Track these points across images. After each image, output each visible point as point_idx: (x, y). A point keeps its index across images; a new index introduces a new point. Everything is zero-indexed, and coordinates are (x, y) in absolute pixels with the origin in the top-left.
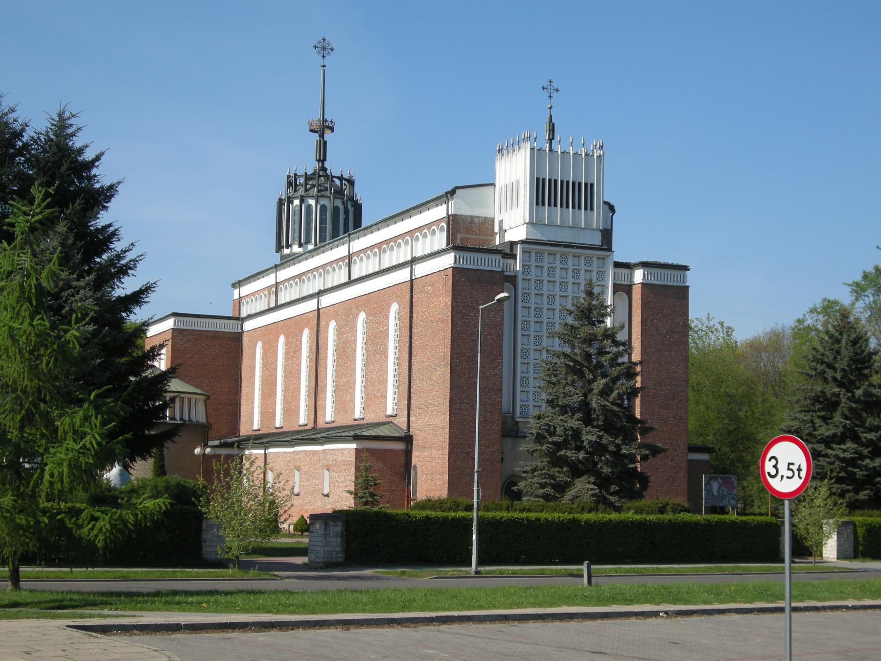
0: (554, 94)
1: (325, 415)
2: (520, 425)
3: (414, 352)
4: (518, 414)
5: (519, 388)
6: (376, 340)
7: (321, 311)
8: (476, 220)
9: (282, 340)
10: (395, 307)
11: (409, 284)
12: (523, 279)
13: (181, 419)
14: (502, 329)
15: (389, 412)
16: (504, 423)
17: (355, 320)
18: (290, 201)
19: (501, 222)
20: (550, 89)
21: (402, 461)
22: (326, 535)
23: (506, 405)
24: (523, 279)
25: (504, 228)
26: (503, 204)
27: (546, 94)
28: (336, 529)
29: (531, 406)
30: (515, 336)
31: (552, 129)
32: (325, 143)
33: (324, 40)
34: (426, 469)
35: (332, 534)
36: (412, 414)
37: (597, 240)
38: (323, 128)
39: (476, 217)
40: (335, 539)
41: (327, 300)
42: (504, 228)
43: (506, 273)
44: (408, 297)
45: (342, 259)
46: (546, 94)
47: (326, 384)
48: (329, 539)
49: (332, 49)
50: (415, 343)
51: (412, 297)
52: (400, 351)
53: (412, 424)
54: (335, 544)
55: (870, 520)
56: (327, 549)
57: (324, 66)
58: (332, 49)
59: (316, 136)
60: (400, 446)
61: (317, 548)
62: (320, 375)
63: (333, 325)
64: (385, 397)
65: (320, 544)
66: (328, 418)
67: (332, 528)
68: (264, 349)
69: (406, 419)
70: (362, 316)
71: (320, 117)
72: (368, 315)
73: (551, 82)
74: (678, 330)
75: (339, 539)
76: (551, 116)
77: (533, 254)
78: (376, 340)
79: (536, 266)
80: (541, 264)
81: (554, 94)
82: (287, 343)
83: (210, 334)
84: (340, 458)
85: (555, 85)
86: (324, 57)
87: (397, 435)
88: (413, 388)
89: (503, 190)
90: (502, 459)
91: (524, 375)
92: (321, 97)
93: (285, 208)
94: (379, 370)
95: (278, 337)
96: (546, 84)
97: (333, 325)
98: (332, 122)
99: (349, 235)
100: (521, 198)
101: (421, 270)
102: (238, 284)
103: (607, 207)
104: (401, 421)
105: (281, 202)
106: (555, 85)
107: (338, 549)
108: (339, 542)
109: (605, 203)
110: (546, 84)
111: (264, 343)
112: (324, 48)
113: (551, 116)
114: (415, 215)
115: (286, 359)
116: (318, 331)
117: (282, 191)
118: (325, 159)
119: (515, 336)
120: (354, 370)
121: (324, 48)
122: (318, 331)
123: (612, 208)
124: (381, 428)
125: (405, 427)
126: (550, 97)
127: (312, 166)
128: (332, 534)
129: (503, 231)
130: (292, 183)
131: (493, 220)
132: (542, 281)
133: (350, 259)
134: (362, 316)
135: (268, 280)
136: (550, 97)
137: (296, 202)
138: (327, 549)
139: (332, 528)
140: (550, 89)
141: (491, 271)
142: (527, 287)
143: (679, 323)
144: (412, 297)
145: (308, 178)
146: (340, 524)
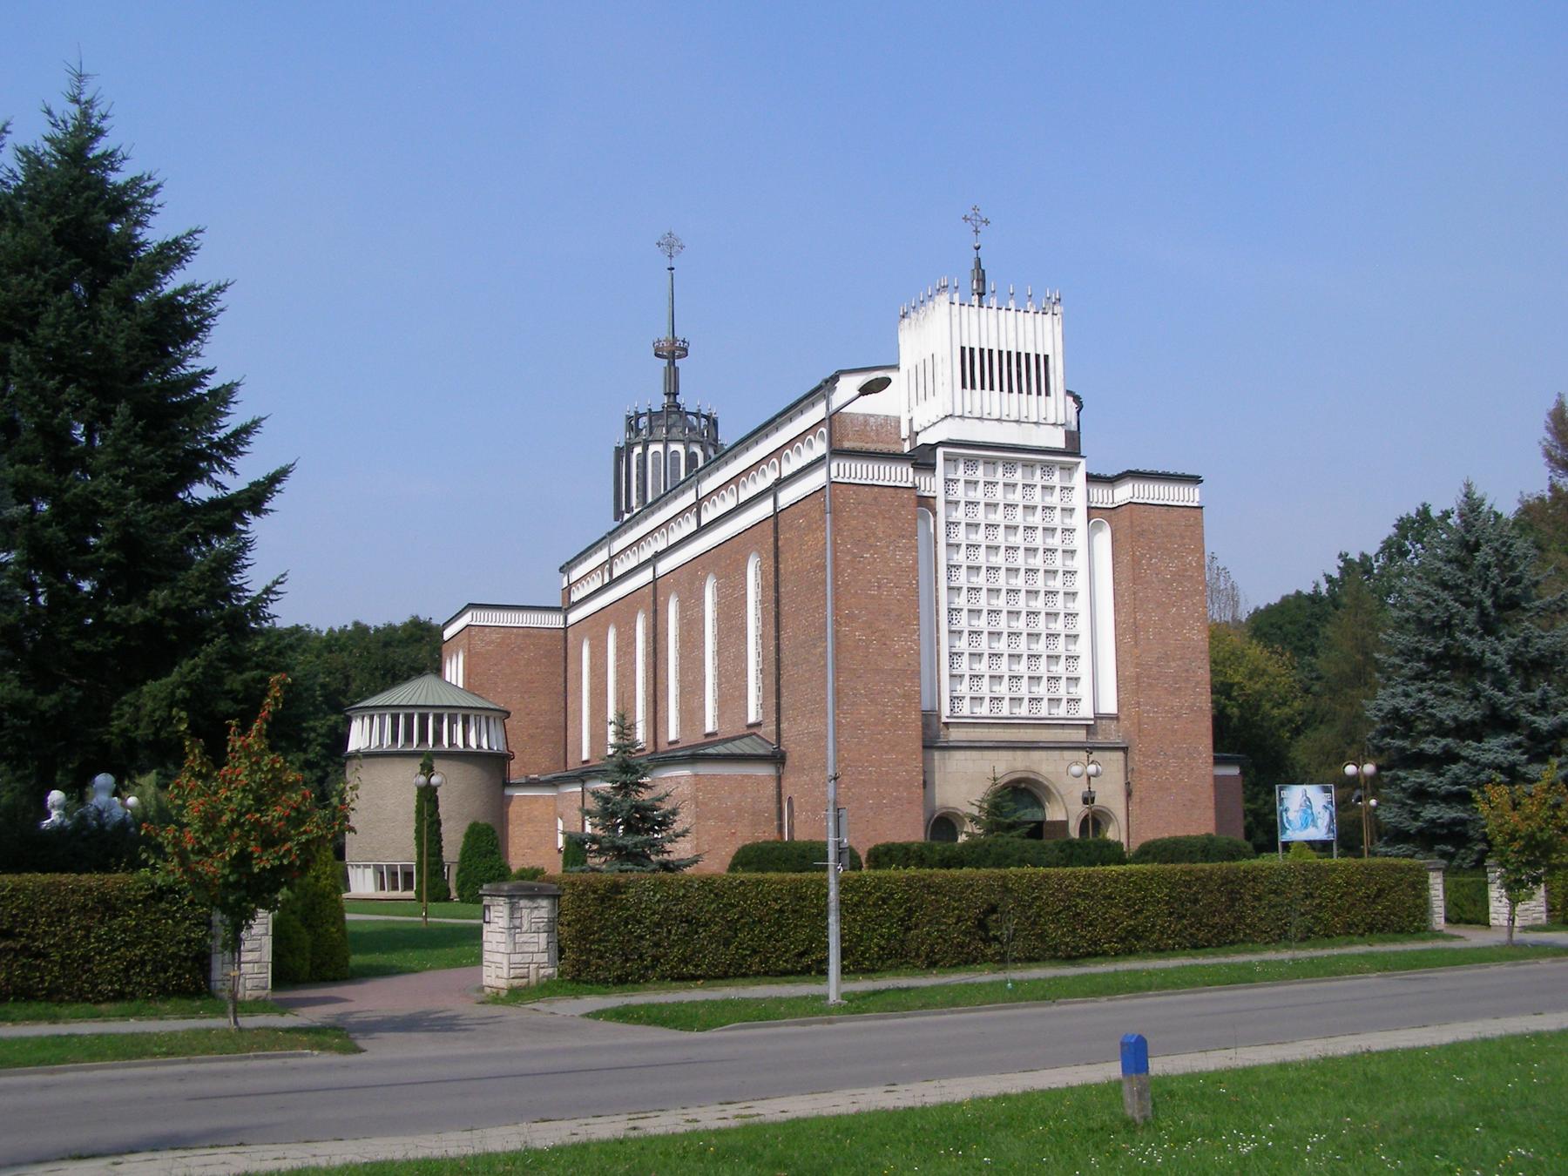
0: (982, 228)
3: (783, 621)
13: (479, 746)
14: (916, 577)
15: (752, 719)
17: (702, 589)
18: (629, 447)
20: (976, 221)
22: (513, 929)
28: (536, 913)
31: (982, 280)
32: (676, 369)
36: (783, 719)
37: (1059, 441)
38: (672, 352)
41: (664, 566)
46: (970, 227)
50: (785, 609)
51: (776, 540)
52: (764, 625)
53: (784, 735)
56: (517, 958)
59: (665, 362)
60: (765, 771)
61: (498, 958)
62: (660, 673)
65: (502, 948)
66: (672, 736)
68: (591, 647)
75: (543, 938)
81: (982, 228)
82: (618, 636)
87: (761, 751)
90: (925, 782)
92: (668, 311)
102: (566, 568)
104: (769, 730)
105: (618, 450)
107: (544, 958)
108: (543, 945)
111: (591, 639)
112: (670, 245)
115: (618, 658)
116: (655, 611)
122: (655, 611)
124: (737, 742)
125: (773, 739)
126: (977, 232)
127: (659, 402)
130: (632, 424)
133: (698, 505)
135: (601, 556)
136: (977, 232)
138: (517, 958)
140: (976, 221)
144: (776, 540)
145: (652, 415)
146: (544, 903)
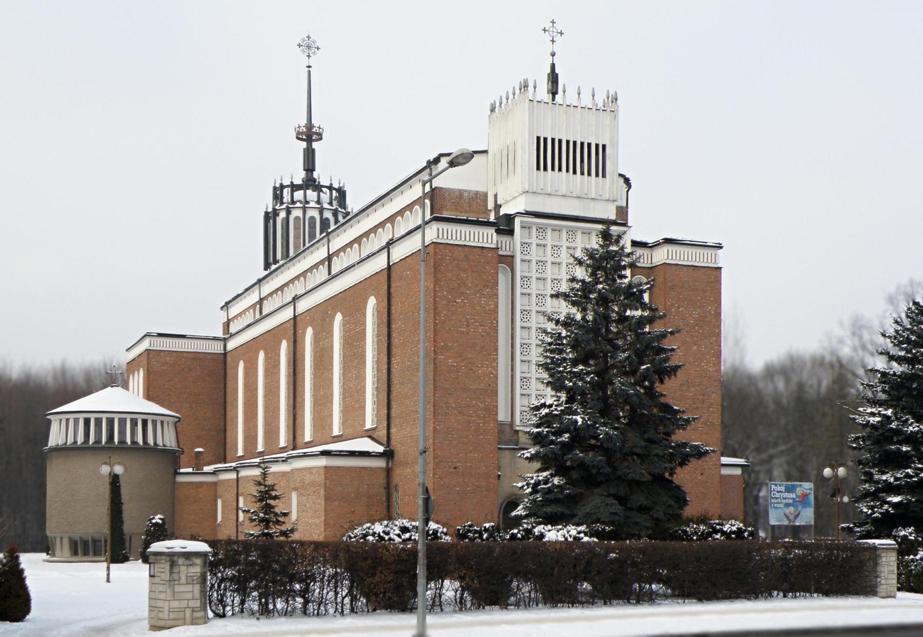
1: (303, 435)
2: (521, 434)
4: (518, 422)
5: (518, 391)
6: (354, 342)
7: (298, 319)
8: (466, 194)
9: (262, 355)
10: (372, 302)
11: (386, 272)
12: (522, 261)
14: (496, 319)
16: (501, 432)
19: (496, 196)
21: (382, 480)
23: (503, 416)
24: (522, 261)
25: (499, 203)
26: (498, 174)
27: (547, 37)
28: (192, 570)
29: (534, 245)
30: (512, 329)
33: (309, 37)
34: (409, 488)
35: (183, 580)
36: (392, 425)
38: (310, 135)
39: (465, 191)
40: (190, 588)
42: (499, 203)
43: (501, 253)
44: (386, 287)
45: (321, 262)
47: (304, 400)
48: (177, 588)
49: (318, 48)
52: (378, 354)
53: (393, 437)
54: (189, 596)
55: (420, 555)
57: (309, 67)
58: (318, 48)
59: (304, 145)
60: (381, 463)
63: (310, 332)
64: (363, 408)
67: (183, 569)
69: (385, 432)
70: (339, 317)
71: (303, 122)
72: (344, 316)
73: (553, 22)
74: (708, 319)
76: (553, 66)
77: (534, 230)
78: (354, 342)
79: (538, 245)
80: (543, 242)
82: (266, 359)
83: (190, 355)
84: (308, 478)
85: (559, 27)
86: (309, 56)
88: (394, 394)
89: (498, 156)
91: (525, 375)
93: (271, 221)
94: (357, 378)
95: (258, 353)
96: (548, 25)
97: (310, 332)
98: (319, 128)
99: (328, 234)
100: (519, 162)
101: (399, 252)
103: (622, 180)
106: (559, 27)
109: (620, 175)
110: (548, 25)
111: (245, 363)
113: (553, 66)
114: (396, 196)
115: (266, 376)
117: (268, 203)
118: (313, 170)
119: (512, 329)
120: (331, 380)
121: (309, 47)
123: (627, 181)
126: (553, 41)
128: (183, 580)
129: (498, 207)
130: (278, 195)
131: (485, 195)
132: (544, 263)
134: (339, 317)
137: (283, 215)
139: (183, 569)
141: (483, 248)
142: (526, 336)
143: (709, 312)
